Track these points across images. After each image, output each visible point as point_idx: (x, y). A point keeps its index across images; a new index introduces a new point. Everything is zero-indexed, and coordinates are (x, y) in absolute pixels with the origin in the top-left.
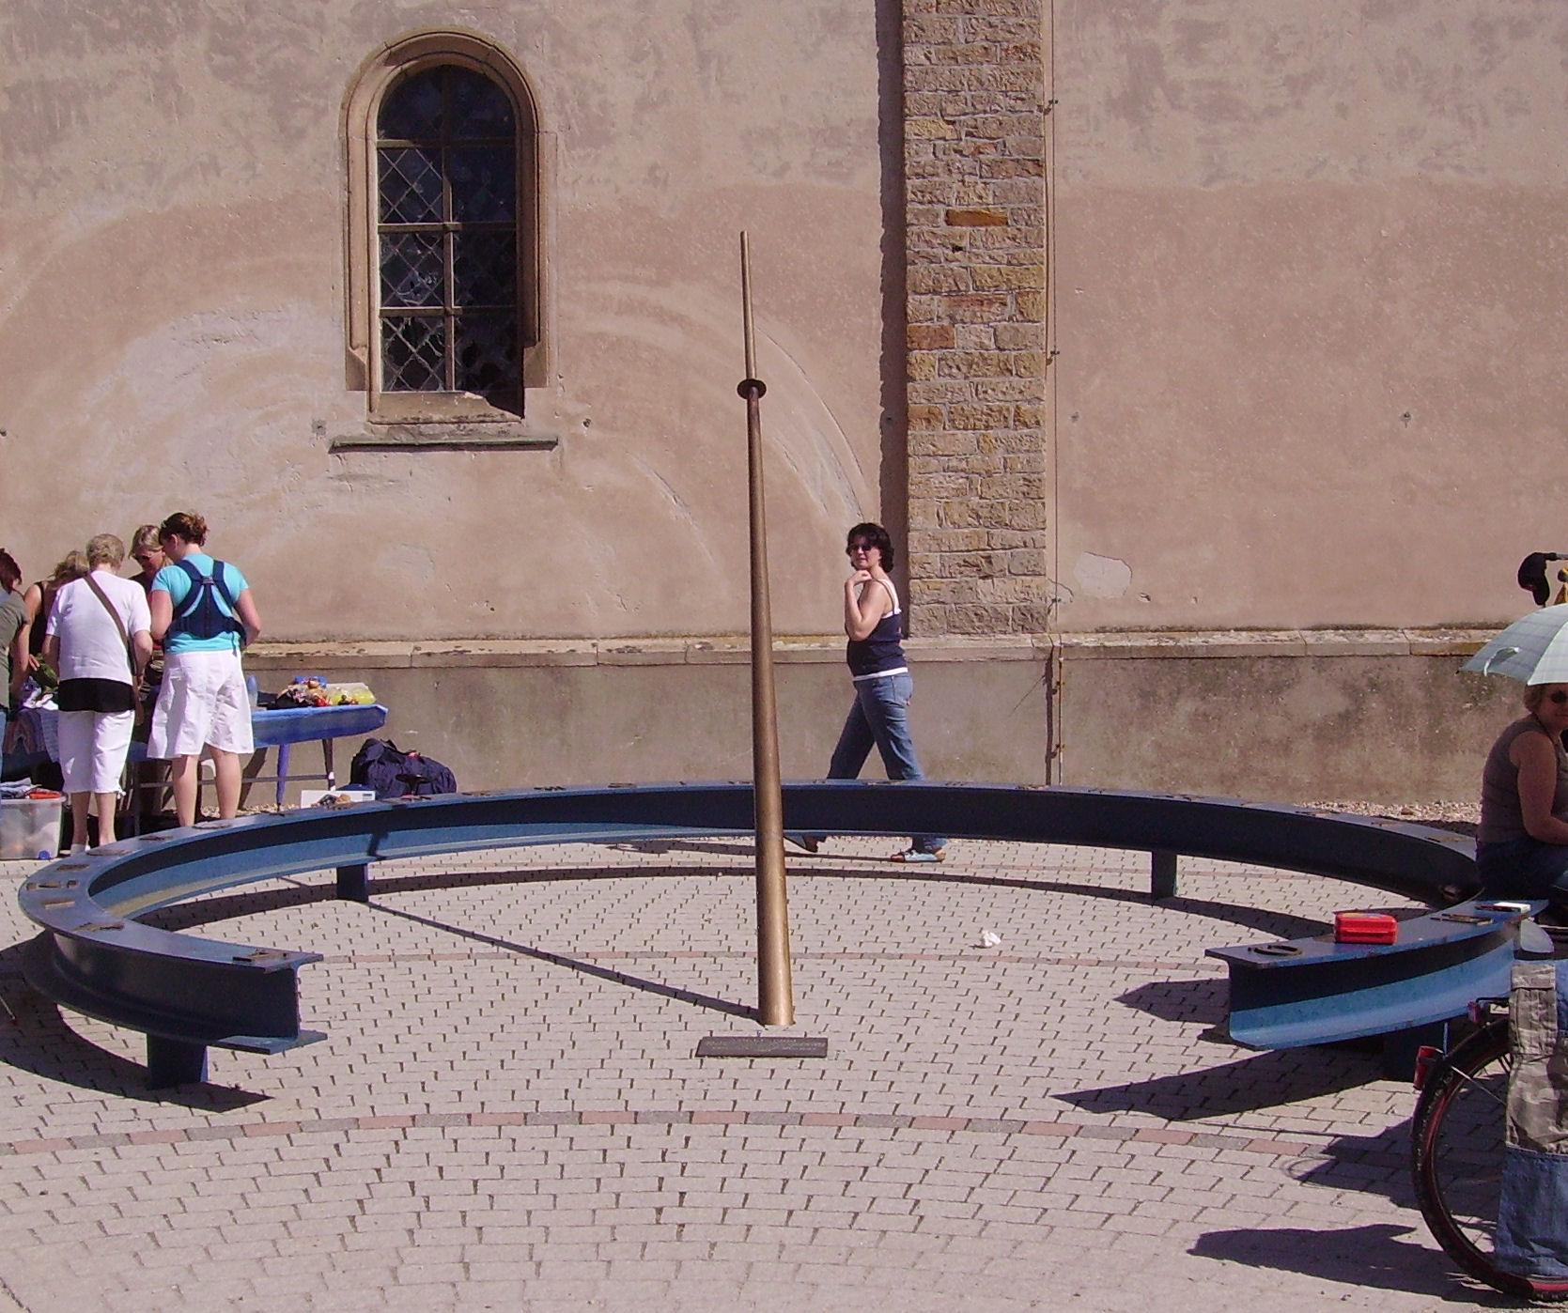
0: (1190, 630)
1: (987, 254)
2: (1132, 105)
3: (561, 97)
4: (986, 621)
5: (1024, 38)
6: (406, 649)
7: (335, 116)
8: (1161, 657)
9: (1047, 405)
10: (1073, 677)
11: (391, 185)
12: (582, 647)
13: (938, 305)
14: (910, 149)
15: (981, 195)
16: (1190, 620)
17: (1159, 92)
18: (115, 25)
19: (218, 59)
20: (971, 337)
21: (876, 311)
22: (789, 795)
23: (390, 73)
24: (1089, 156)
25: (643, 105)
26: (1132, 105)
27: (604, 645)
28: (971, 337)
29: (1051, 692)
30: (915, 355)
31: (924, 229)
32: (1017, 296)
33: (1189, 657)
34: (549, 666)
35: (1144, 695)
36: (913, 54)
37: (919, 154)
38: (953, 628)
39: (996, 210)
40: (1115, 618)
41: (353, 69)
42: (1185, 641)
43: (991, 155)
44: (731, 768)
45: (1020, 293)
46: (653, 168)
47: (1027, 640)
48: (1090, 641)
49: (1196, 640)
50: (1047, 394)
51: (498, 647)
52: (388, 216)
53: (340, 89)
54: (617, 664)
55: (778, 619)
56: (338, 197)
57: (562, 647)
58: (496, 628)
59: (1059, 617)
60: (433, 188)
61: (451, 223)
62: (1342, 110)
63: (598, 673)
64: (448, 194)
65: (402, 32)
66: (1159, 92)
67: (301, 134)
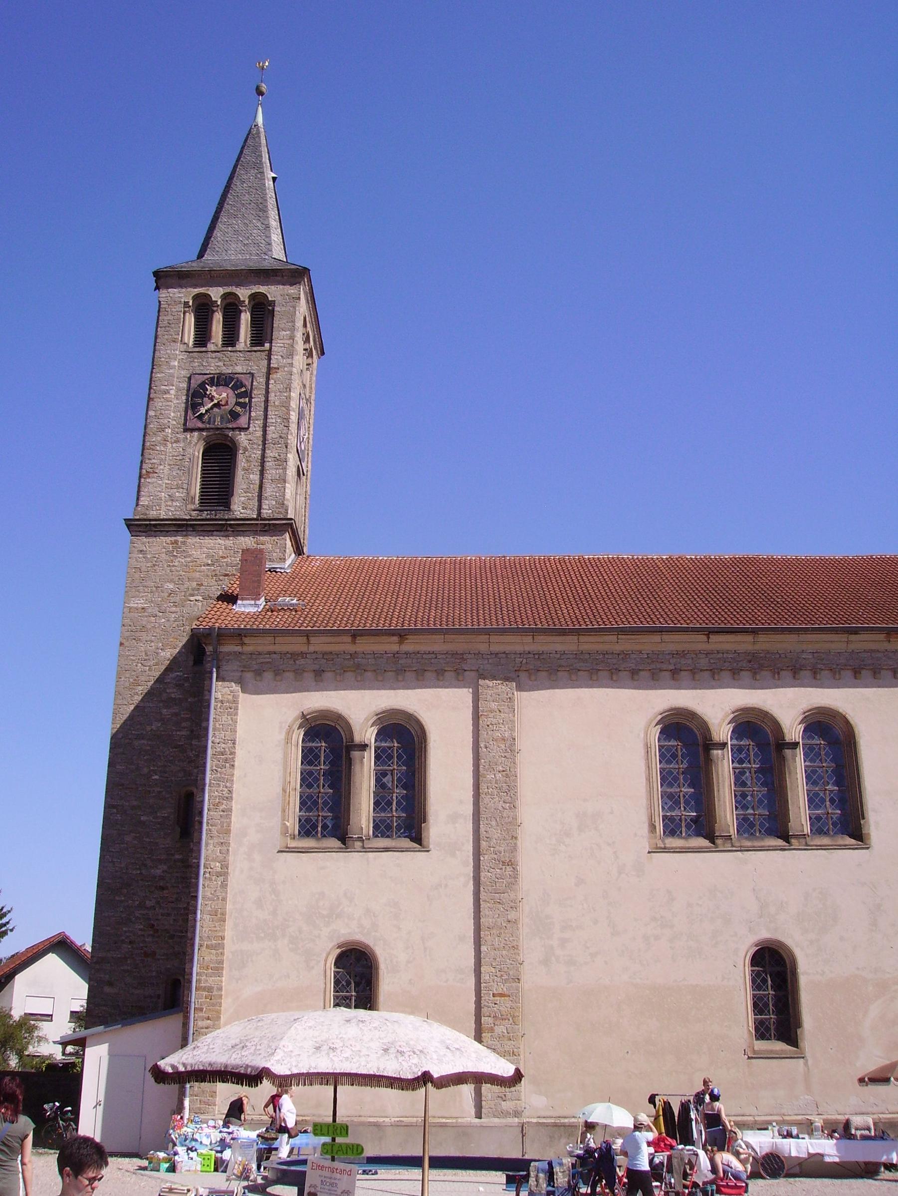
0: (565, 1117)
1: (504, 1005)
2: (546, 962)
3: (386, 960)
4: (505, 1114)
5: (515, 943)
6: (751, 1118)
7: (323, 963)
8: (555, 1125)
9: (521, 1050)
10: (530, 1132)
11: (337, 982)
12: (387, 1120)
13: (490, 1020)
14: (482, 975)
15: (502, 988)
16: (565, 1114)
17: (553, 959)
18: (262, 935)
19: (291, 946)
20: (500, 1029)
21: (473, 1022)
22: (431, 1158)
23: (339, 951)
24: (533, 977)
25: (408, 962)
26: (546, 962)
27: (393, 1119)
28: (500, 1029)
29: (523, 1136)
30: (483, 1035)
31: (486, 998)
32: (513, 1017)
33: (564, 1125)
34: (377, 1125)
35: (550, 1137)
36: (484, 948)
37: (485, 977)
38: (495, 1116)
39: (507, 993)
40: (543, 1114)
41: (328, 950)
42: (563, 1121)
43: (506, 977)
44: (418, 1153)
45: (513, 1017)
46: (410, 980)
47: (516, 1120)
48: (534, 1120)
49: (566, 1120)
50: (522, 1046)
51: (362, 1119)
52: (336, 991)
53: (324, 955)
54: (398, 1125)
55: (431, 1113)
56: (323, 986)
57: (381, 1120)
58: (362, 1114)
59: (526, 1113)
60: (349, 983)
61: (354, 994)
62: (606, 963)
63: (391, 1128)
64: (353, 985)
65: (342, 940)
66: (553, 959)
67: (313, 968)
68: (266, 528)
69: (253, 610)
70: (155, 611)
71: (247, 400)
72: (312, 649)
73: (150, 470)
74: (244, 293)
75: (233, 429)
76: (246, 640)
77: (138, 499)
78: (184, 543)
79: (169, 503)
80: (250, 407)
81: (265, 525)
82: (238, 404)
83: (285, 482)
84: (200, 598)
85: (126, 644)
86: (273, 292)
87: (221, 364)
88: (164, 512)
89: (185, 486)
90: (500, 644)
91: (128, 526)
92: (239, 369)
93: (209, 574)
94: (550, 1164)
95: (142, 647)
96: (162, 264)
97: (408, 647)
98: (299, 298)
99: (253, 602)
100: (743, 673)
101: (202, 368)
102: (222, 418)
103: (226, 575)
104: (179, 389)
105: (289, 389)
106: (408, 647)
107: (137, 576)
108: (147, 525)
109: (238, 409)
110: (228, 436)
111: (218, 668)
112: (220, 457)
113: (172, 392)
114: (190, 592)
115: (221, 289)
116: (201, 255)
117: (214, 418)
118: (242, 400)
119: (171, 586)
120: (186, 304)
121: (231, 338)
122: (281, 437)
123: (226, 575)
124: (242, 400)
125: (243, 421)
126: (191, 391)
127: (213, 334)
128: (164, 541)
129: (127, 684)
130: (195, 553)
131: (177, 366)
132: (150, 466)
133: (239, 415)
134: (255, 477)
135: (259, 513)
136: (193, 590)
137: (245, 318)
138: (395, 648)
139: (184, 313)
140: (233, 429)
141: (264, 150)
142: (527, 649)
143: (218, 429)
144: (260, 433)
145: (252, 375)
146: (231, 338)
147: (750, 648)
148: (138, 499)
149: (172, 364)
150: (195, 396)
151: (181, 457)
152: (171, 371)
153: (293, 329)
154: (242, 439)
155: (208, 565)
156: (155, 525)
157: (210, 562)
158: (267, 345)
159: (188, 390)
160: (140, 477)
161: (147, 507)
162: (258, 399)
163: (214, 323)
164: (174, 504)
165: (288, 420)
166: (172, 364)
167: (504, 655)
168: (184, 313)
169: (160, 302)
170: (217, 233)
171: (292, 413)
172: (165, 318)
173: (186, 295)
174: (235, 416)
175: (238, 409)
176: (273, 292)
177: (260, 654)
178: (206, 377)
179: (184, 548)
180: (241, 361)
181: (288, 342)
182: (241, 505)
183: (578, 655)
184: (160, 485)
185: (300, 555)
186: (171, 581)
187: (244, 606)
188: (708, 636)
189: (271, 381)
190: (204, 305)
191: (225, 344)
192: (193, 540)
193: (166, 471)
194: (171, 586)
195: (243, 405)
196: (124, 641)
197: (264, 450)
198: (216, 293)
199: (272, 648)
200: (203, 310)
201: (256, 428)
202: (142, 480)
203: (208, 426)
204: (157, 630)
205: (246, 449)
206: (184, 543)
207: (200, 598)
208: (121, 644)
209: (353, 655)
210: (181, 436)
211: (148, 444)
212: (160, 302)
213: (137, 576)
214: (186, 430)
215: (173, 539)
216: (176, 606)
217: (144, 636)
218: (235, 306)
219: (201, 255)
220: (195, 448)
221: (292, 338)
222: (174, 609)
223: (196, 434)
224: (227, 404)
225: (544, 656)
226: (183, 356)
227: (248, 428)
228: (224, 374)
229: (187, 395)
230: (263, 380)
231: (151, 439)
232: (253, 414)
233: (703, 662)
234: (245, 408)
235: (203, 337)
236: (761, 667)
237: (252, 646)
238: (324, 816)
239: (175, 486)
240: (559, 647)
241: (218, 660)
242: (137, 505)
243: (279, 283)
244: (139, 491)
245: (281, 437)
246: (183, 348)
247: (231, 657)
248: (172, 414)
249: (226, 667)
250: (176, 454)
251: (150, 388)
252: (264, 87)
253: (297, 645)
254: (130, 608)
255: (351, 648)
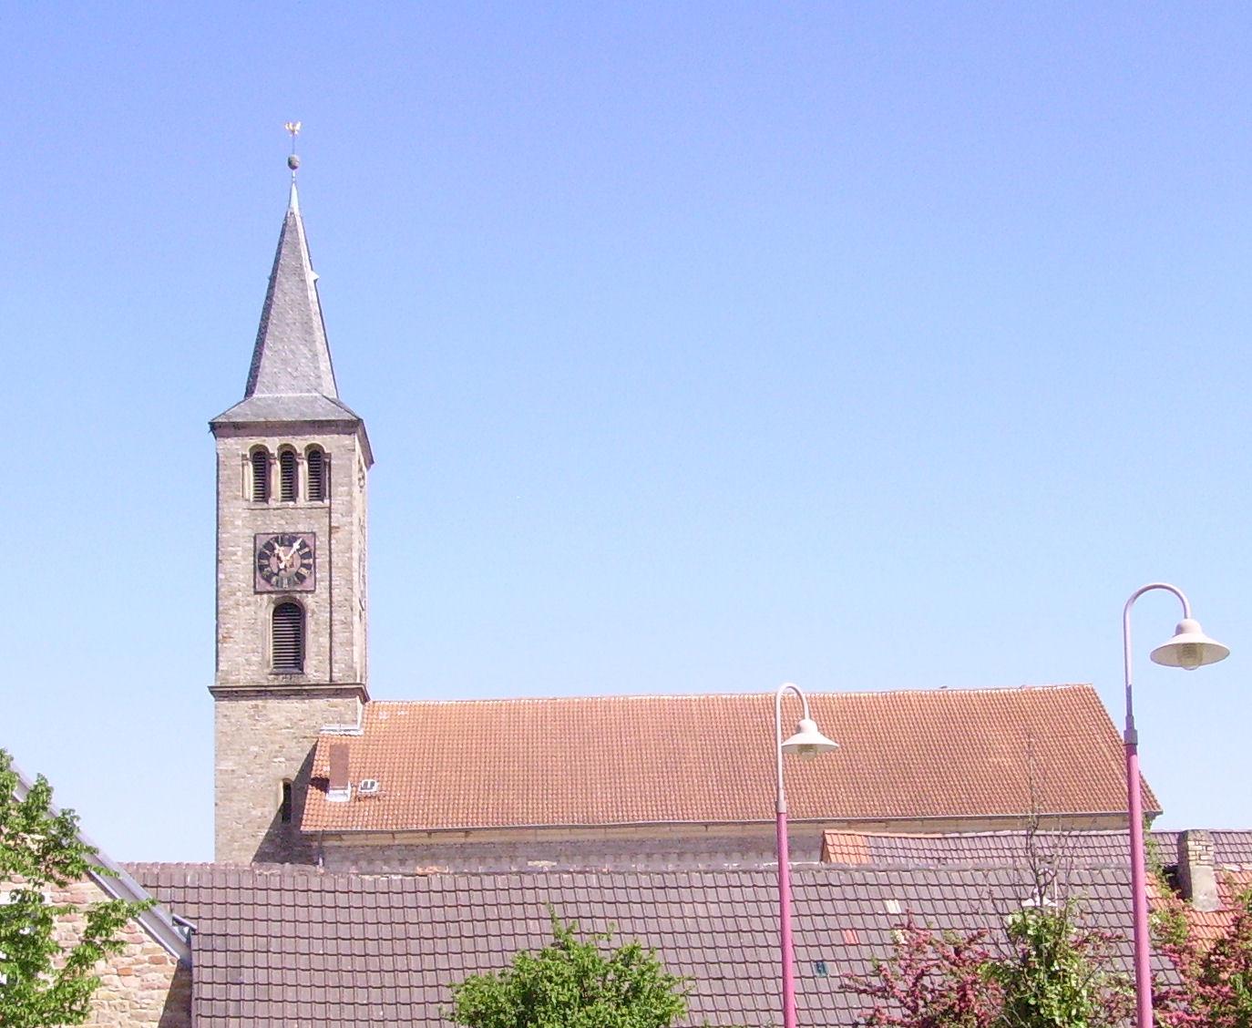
68: (338, 692)
69: (344, 799)
70: (244, 772)
71: (311, 561)
72: (396, 842)
73: (225, 635)
74: (300, 444)
75: (300, 592)
76: (344, 837)
77: (217, 664)
78: (264, 707)
79: (247, 667)
80: (315, 567)
81: (337, 689)
82: (303, 565)
83: (353, 645)
84: (283, 759)
85: (220, 804)
86: (327, 442)
87: (283, 522)
88: (243, 678)
89: (260, 650)
90: (543, 836)
91: (212, 692)
92: (301, 528)
93: (290, 736)
94: (171, 875)
95: (235, 806)
96: (214, 413)
97: (470, 840)
98: (354, 450)
99: (342, 792)
100: (734, 854)
101: (265, 526)
102: (289, 580)
103: (305, 737)
104: (245, 550)
105: (350, 549)
106: (470, 840)
107: (223, 739)
108: (228, 692)
109: (304, 571)
110: (295, 599)
111: (323, 859)
112: (290, 613)
113: (240, 553)
114: (274, 754)
115: (276, 438)
116: (250, 391)
117: (282, 579)
118: (306, 561)
119: (255, 749)
120: (244, 456)
121: (290, 493)
122: (346, 600)
123: (305, 737)
124: (306, 561)
125: (308, 584)
126: (258, 552)
127: (273, 489)
128: (245, 704)
129: (225, 841)
130: (275, 717)
131: (244, 525)
132: (226, 631)
133: (304, 577)
134: (325, 640)
135: (331, 680)
136: (277, 751)
137: (303, 469)
138: (463, 840)
139: (243, 465)
140: (300, 592)
141: (303, 247)
142: (566, 838)
143: (286, 592)
144: (326, 595)
145: (314, 534)
146: (290, 493)
147: (740, 835)
148: (217, 664)
149: (236, 523)
150: (263, 555)
151: (253, 621)
152: (236, 531)
153: (350, 484)
154: (309, 601)
155: (288, 728)
156: (236, 692)
157: (289, 725)
158: (327, 502)
159: (255, 551)
160: (217, 642)
161: (228, 673)
162: (322, 559)
163: (273, 477)
164: (252, 668)
165: (351, 581)
166: (236, 523)
167: (547, 844)
168: (243, 465)
169: (217, 454)
170: (265, 362)
171: (354, 574)
172: (225, 472)
173: (243, 445)
174: (301, 578)
175: (304, 571)
176: (327, 442)
177: (355, 846)
178: (273, 536)
179: (264, 712)
180: (299, 516)
181: (345, 498)
182: (314, 670)
183: (605, 843)
184: (237, 650)
185: (366, 701)
186: (256, 744)
187: (336, 795)
188: (706, 826)
189: (333, 541)
190: (258, 453)
191: (285, 499)
192: (272, 703)
193: (242, 635)
194: (255, 749)
195: (308, 567)
196: (218, 802)
197: (331, 612)
198: (273, 444)
199: (364, 842)
200: (260, 459)
201: (322, 587)
202: (220, 645)
203: (277, 589)
204: (247, 791)
205: (313, 612)
206: (264, 707)
207: (283, 759)
208: (216, 805)
209: (429, 847)
210: (252, 599)
211: (221, 608)
212: (217, 454)
213: (223, 739)
214: (256, 593)
215: (254, 702)
216: (262, 768)
217: (235, 796)
218: (291, 460)
219: (250, 391)
220: (263, 610)
221: (350, 494)
222: (260, 770)
223: (265, 596)
224: (292, 566)
225: (578, 844)
226: (246, 514)
227: (314, 591)
228: (287, 534)
229: (254, 556)
230: (324, 539)
231: (224, 603)
232: (318, 576)
233: (703, 846)
234: (310, 569)
235: (263, 493)
236: (748, 850)
237: (347, 841)
238: (246, 455)
239: (252, 655)
240: (591, 838)
241: (323, 853)
242: (217, 670)
243: (333, 433)
244: (217, 656)
245: (346, 600)
246: (245, 505)
247: (332, 851)
248: (242, 577)
249: (329, 858)
250: (248, 617)
251: (218, 549)
252: (297, 158)
253: (386, 841)
254: (221, 770)
255: (427, 841)
